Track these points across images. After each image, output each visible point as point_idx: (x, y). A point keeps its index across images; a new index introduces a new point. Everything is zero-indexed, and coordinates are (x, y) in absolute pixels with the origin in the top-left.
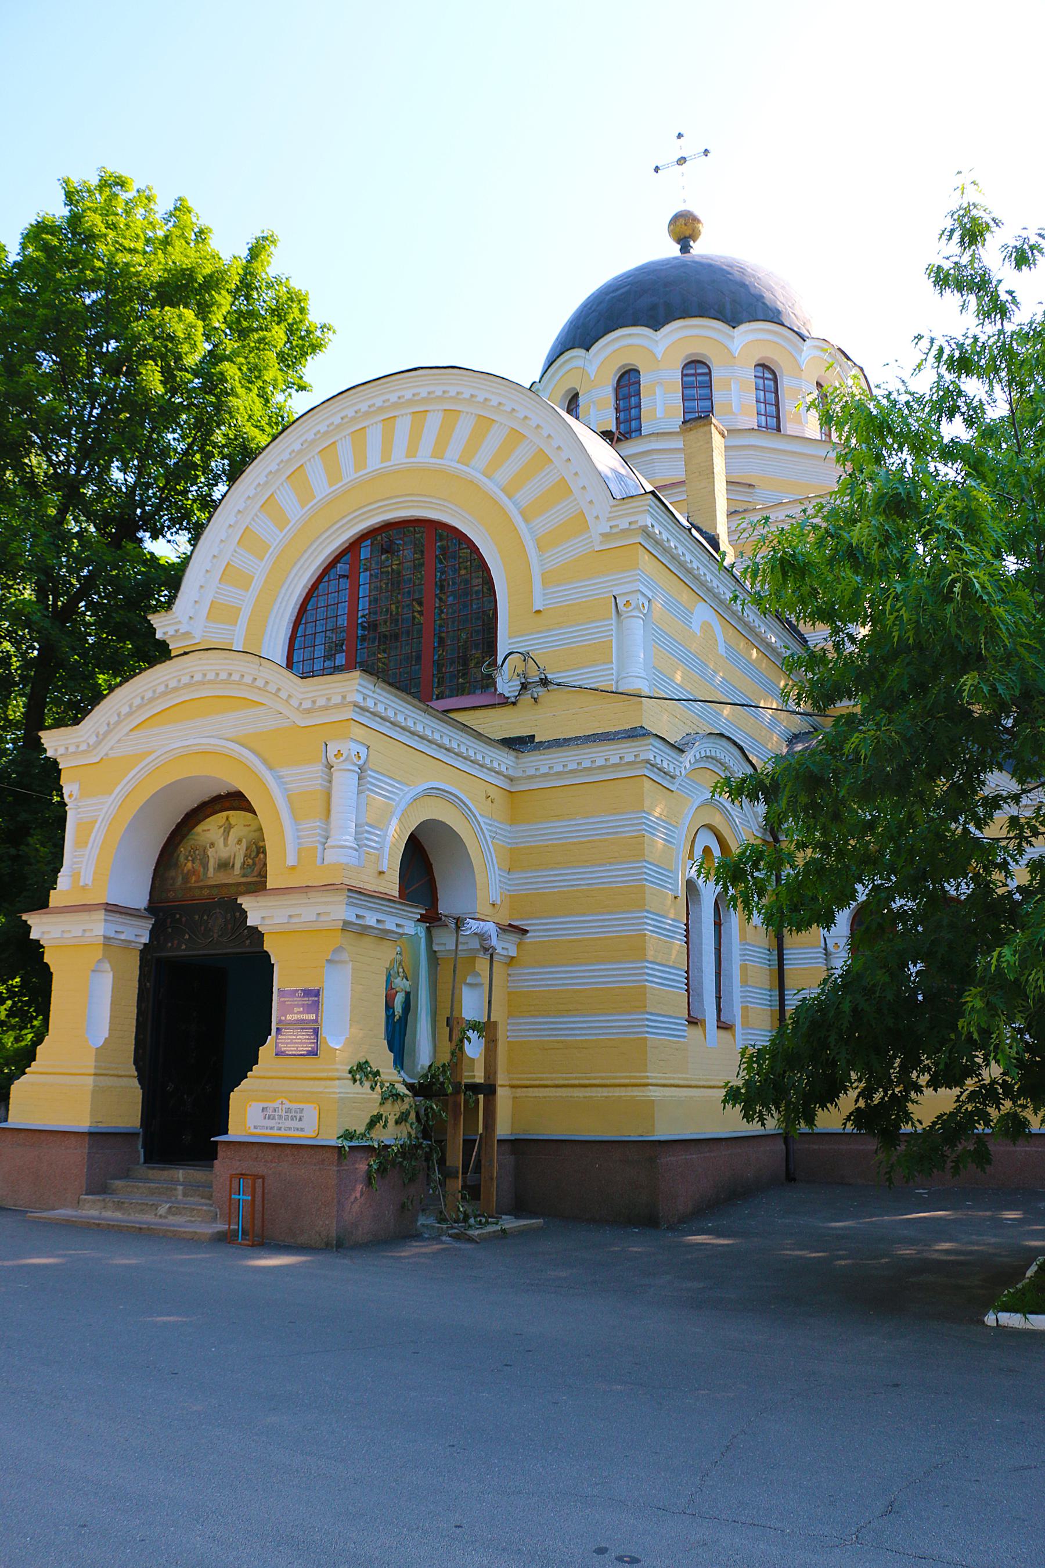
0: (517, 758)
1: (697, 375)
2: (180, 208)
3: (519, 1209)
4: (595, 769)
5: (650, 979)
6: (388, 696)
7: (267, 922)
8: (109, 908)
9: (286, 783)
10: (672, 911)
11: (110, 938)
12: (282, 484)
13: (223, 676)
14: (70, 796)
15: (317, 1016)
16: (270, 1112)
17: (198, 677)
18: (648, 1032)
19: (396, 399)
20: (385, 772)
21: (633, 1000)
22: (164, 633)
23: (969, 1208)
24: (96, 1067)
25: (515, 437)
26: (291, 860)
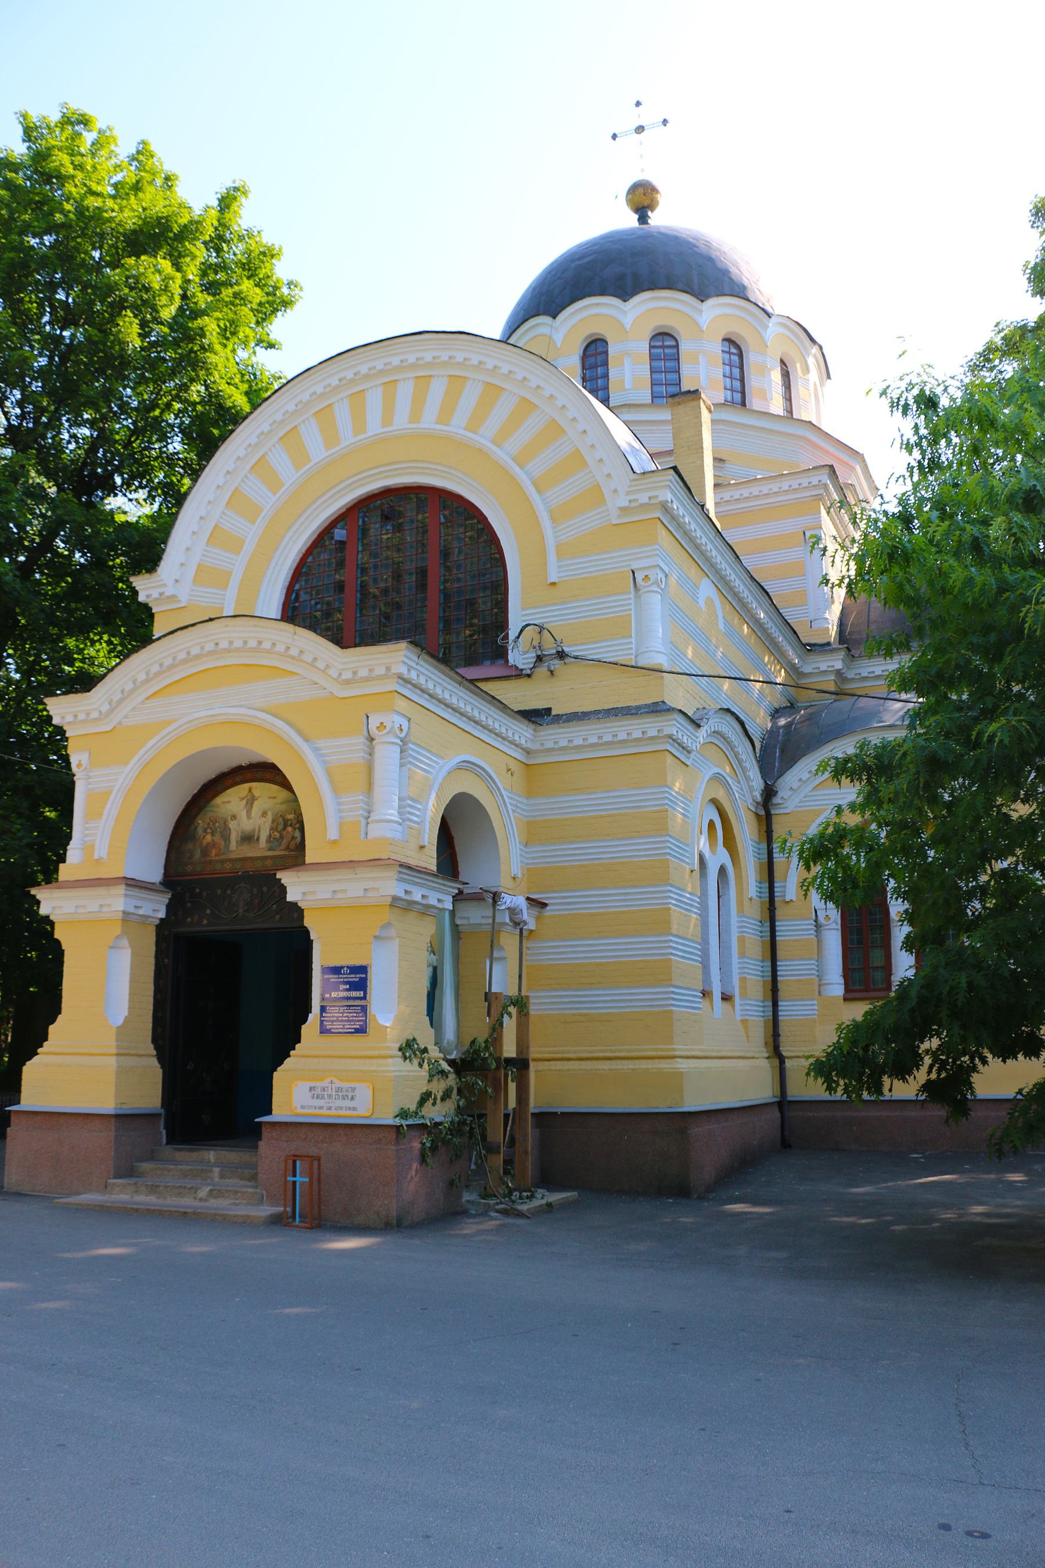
0: (535, 730)
1: (665, 346)
2: (142, 155)
3: (547, 1180)
4: (602, 745)
5: (675, 952)
6: (429, 667)
7: (309, 897)
8: (129, 882)
9: (323, 755)
10: (690, 885)
11: (129, 913)
12: (274, 446)
13: (253, 644)
14: (79, 765)
15: (365, 994)
16: (318, 1091)
17: (224, 644)
18: (673, 1005)
19: (398, 363)
20: (423, 744)
21: (659, 973)
22: (148, 596)
23: (970, 1171)
24: (118, 1047)
25: (526, 407)
26: (333, 834)
